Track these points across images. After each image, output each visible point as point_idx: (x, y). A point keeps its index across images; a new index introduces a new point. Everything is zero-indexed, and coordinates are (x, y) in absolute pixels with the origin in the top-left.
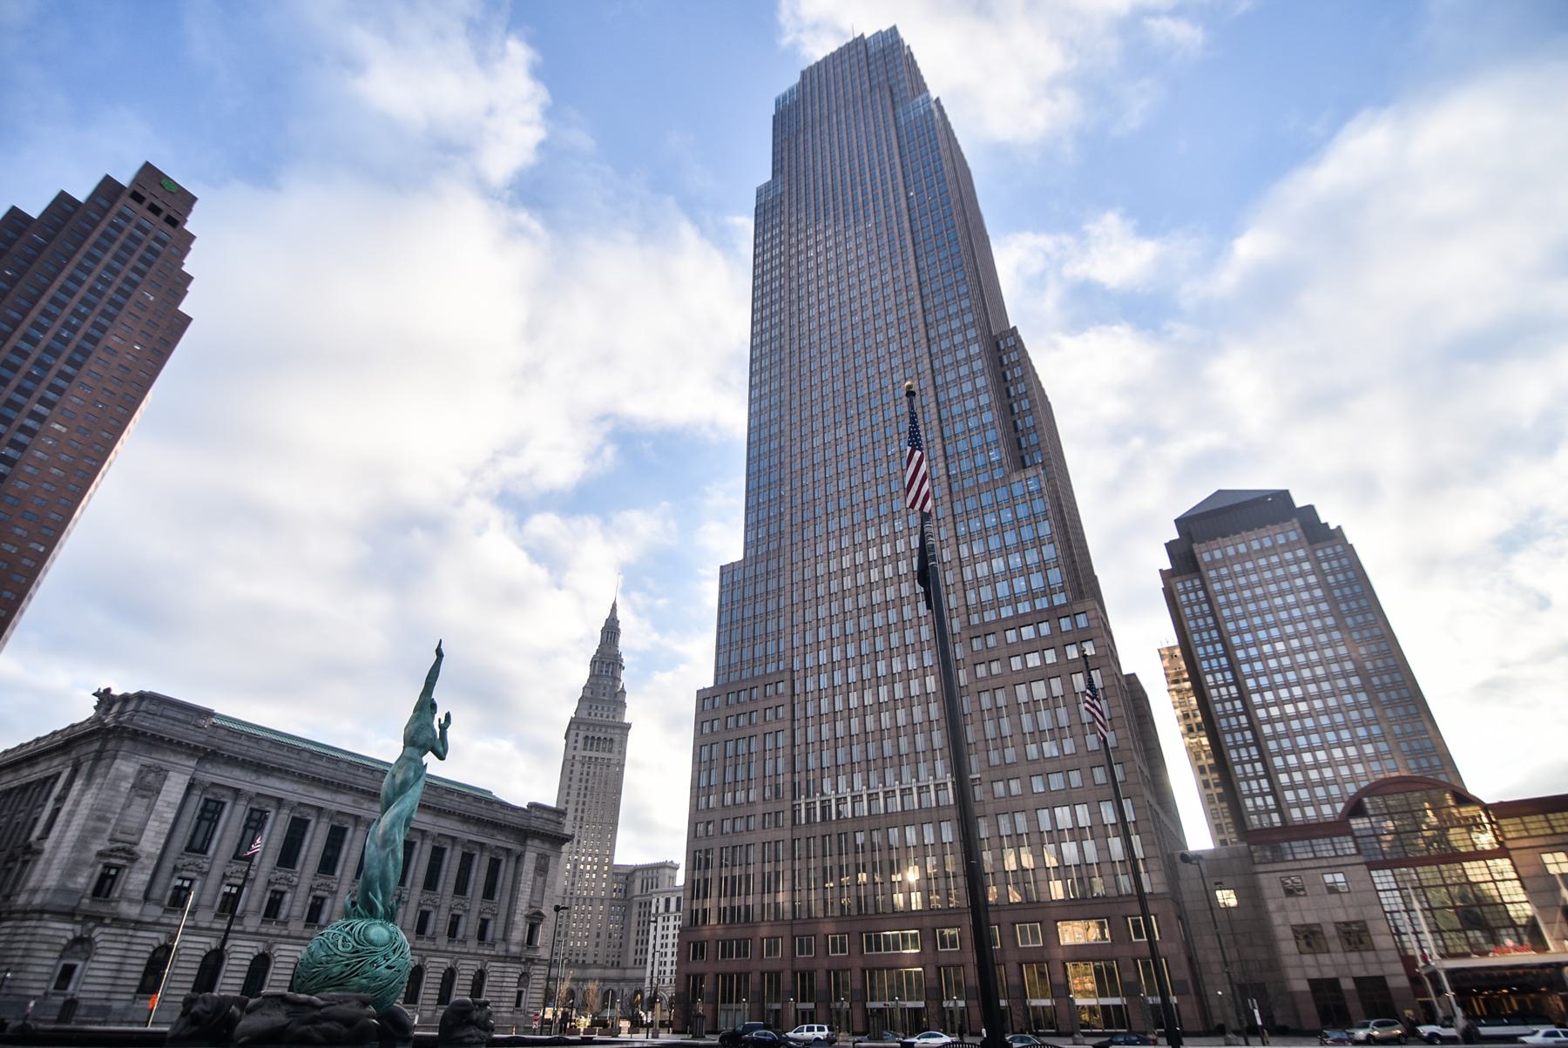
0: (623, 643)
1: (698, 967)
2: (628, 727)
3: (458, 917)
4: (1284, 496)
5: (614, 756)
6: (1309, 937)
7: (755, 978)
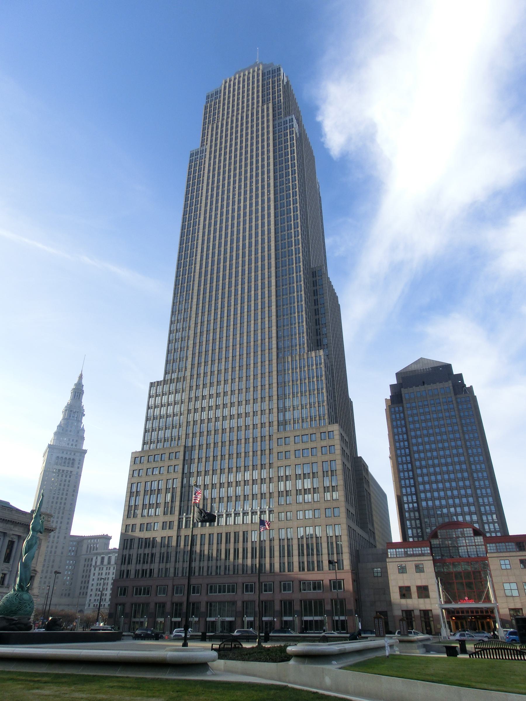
0: (86, 401)
1: (122, 599)
2: (85, 452)
3: (5, 575)
4: (448, 367)
5: (75, 470)
6: (405, 592)
7: (152, 606)
